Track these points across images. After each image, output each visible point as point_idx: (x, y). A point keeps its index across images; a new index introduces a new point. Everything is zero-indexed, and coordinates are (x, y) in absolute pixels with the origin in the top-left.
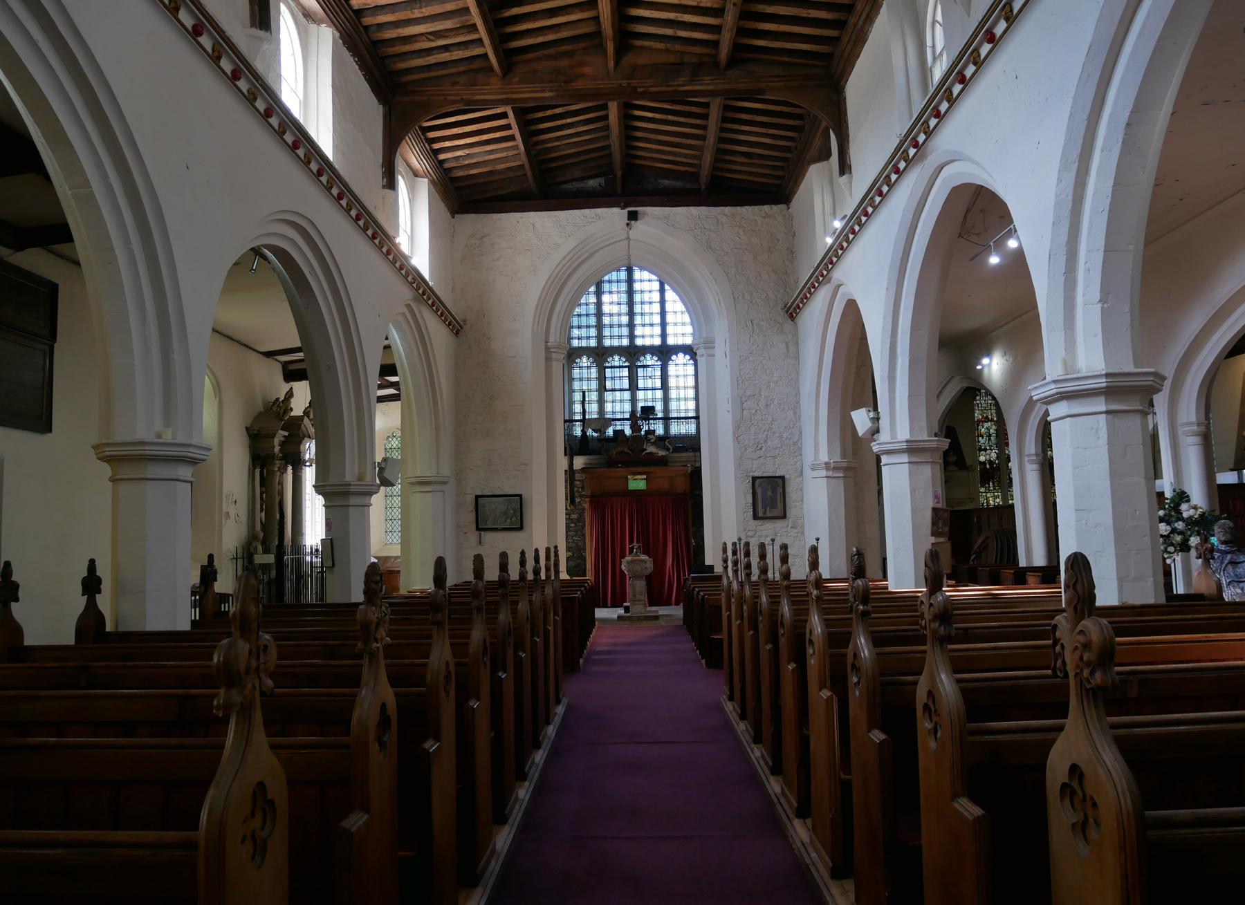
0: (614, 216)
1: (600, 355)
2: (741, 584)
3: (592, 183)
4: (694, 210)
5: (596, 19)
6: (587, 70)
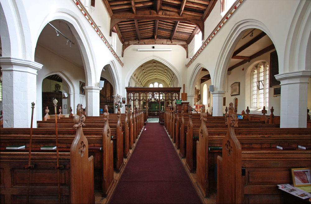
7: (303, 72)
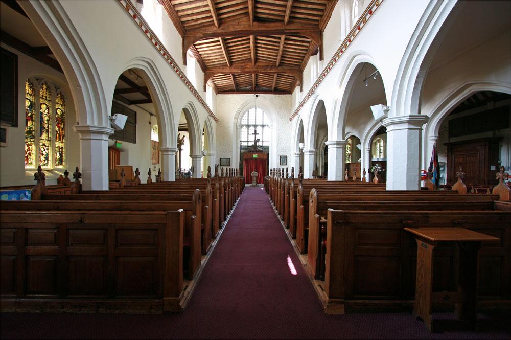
0: (253, 96)
1: (248, 126)
2: (281, 179)
3: (248, 88)
4: (270, 95)
5: (251, 56)
6: (248, 66)
7: (410, 116)
